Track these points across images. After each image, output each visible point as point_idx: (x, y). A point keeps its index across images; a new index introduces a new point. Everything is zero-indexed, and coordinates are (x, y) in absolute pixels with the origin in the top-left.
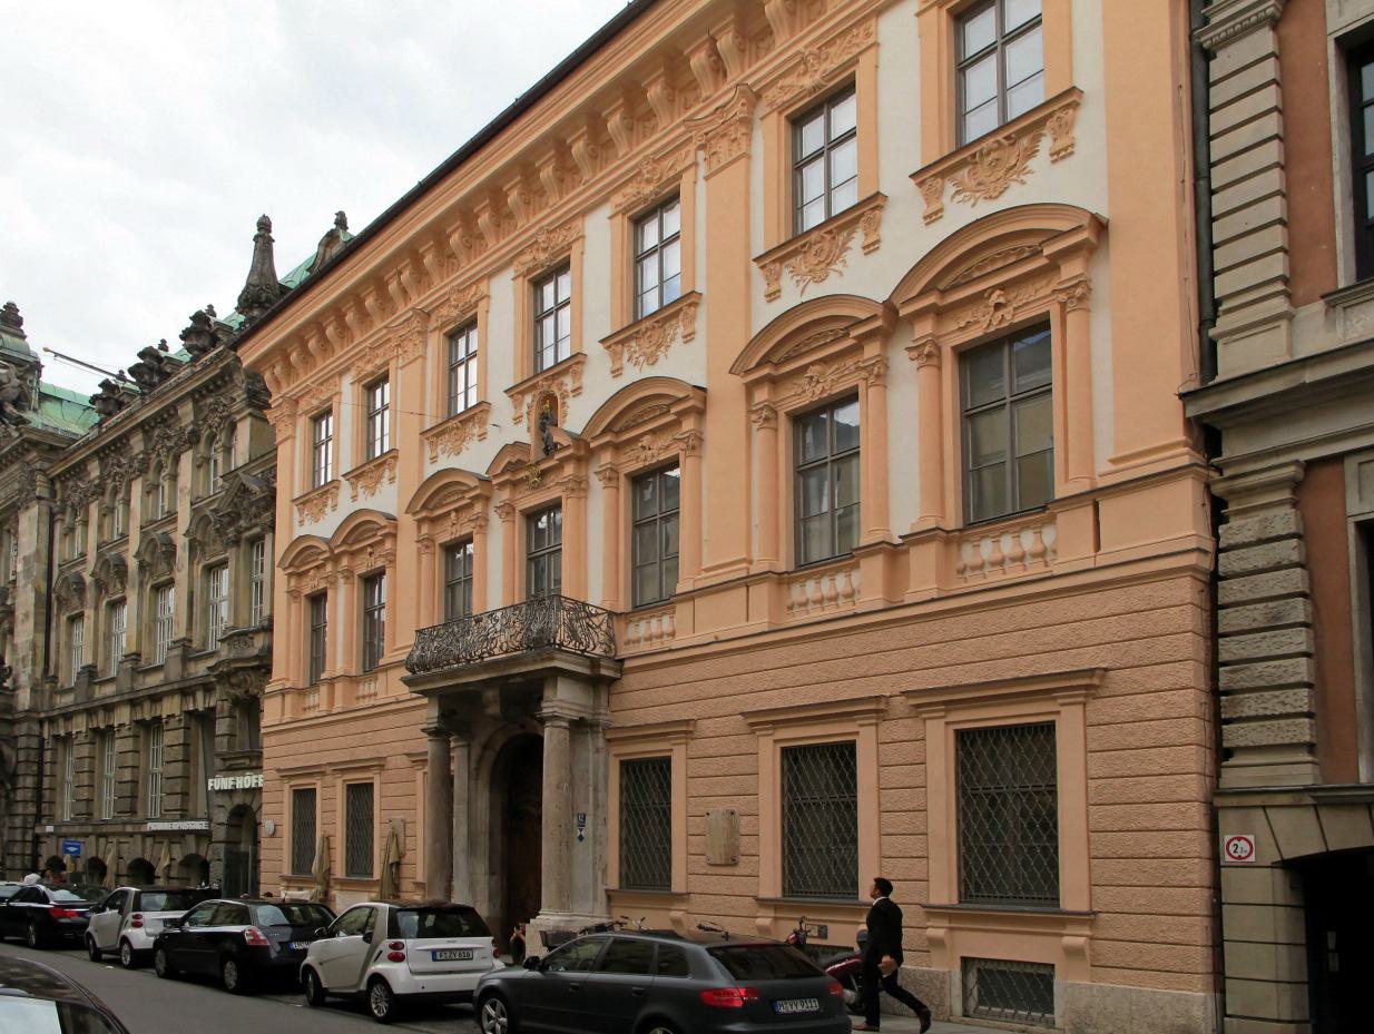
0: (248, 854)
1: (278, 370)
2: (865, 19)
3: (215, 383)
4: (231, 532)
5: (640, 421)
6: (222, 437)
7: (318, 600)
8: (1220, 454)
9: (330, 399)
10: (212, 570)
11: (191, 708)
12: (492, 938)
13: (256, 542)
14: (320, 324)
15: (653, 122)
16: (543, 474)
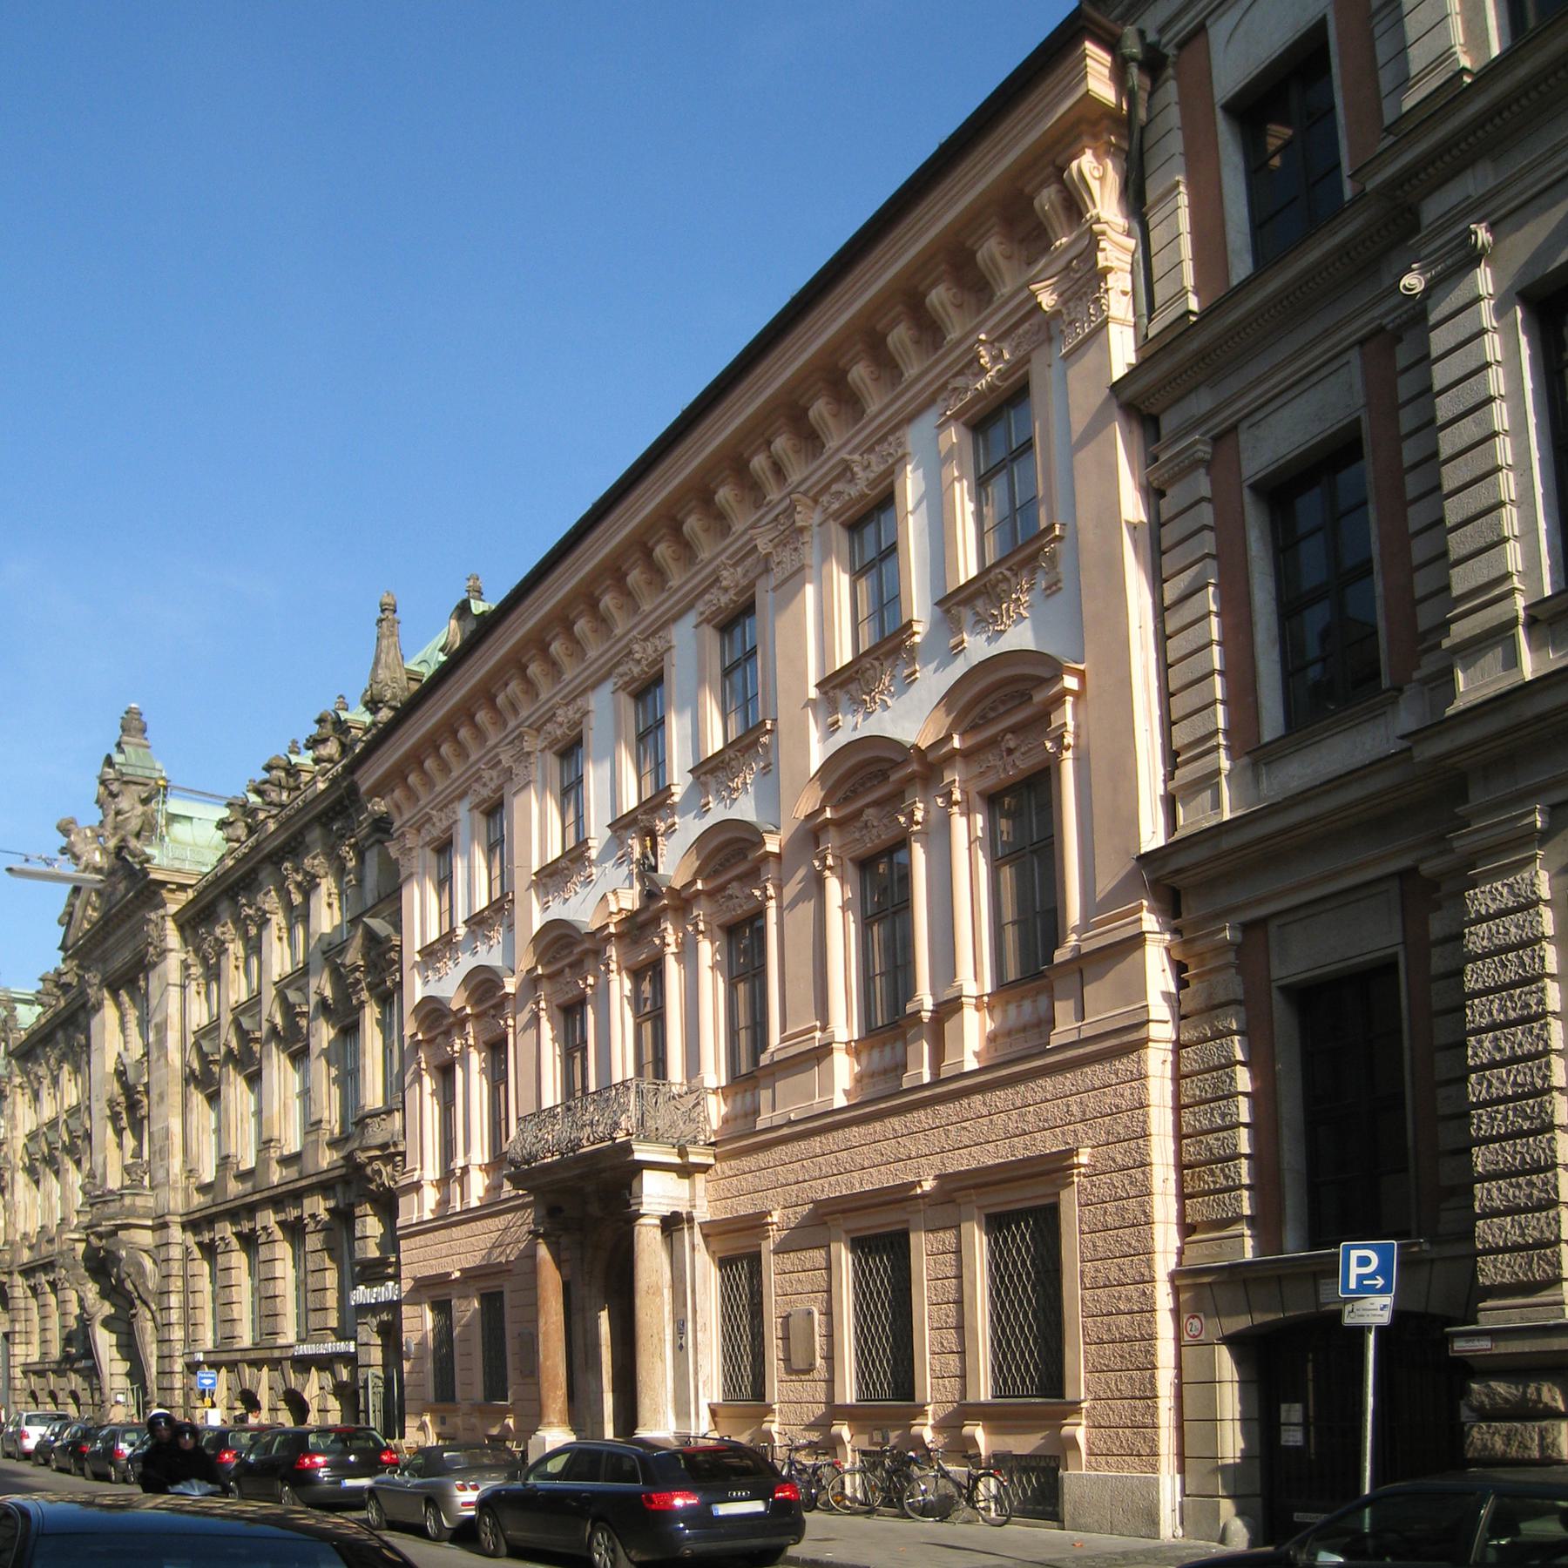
0: (1476, 1322)
1: (781, 443)
2: (452, 801)
5: (992, 715)
8: (1466, 800)
9: (450, 828)
14: (645, 544)
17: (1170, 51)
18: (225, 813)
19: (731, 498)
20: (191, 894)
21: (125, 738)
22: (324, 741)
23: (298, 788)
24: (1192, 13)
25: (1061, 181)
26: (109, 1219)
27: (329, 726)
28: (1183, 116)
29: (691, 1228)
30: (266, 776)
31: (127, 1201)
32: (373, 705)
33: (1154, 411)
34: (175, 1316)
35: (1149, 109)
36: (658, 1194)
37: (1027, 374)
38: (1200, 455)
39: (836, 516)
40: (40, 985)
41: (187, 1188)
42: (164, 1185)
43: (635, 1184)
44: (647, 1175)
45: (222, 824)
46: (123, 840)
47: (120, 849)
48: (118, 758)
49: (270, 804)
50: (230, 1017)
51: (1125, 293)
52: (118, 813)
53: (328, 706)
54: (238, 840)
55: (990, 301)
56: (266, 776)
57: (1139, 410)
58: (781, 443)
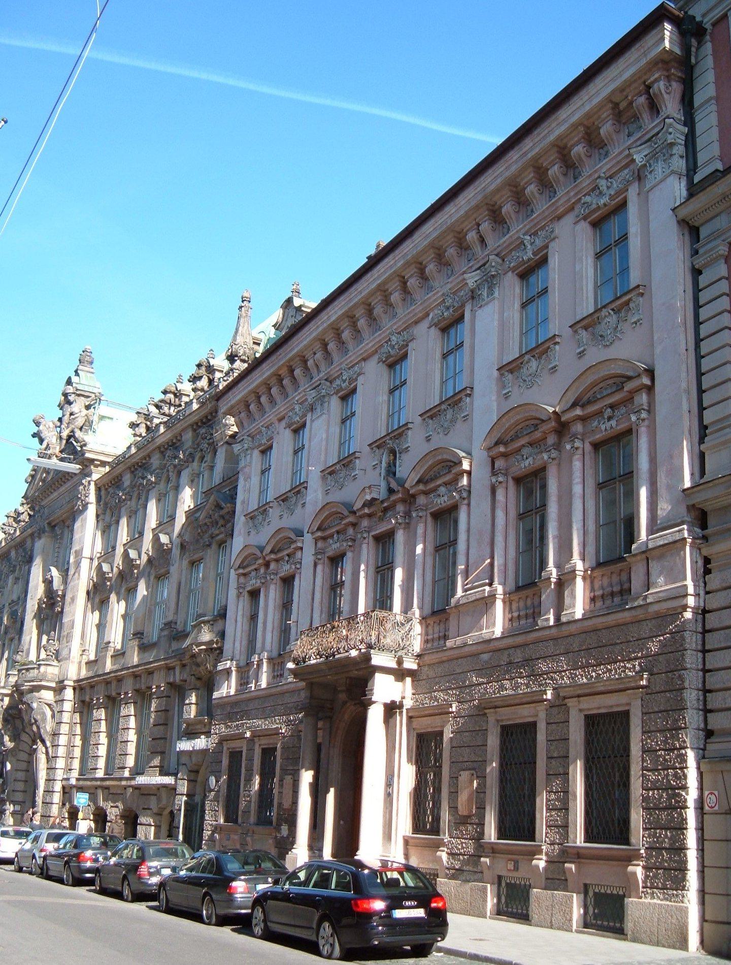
3: (206, 417)
4: (206, 538)
6: (208, 458)
7: (254, 594)
10: (193, 564)
11: (171, 680)
12: (356, 857)
13: (221, 544)
15: (605, 149)
16: (386, 510)
17: (708, 26)
18: (134, 418)
19: (455, 253)
20: (107, 469)
21: (81, 367)
22: (200, 378)
23: (180, 405)
24: (720, 8)
25: (648, 93)
26: (29, 681)
27: (204, 368)
28: (715, 62)
29: (401, 713)
30: (162, 396)
31: (42, 669)
32: (231, 358)
33: (696, 224)
34: (61, 751)
35: (696, 57)
36: (384, 689)
37: (626, 197)
38: (721, 252)
39: (513, 270)
40: (5, 520)
41: (80, 662)
42: (66, 659)
43: (369, 684)
44: (379, 677)
45: (133, 425)
46: (72, 431)
47: (71, 436)
48: (75, 379)
49: (164, 414)
50: (122, 550)
51: (682, 157)
52: (71, 414)
53: (202, 357)
54: (140, 436)
55: (606, 155)
56: (162, 396)
57: (688, 223)
58: (485, 227)
